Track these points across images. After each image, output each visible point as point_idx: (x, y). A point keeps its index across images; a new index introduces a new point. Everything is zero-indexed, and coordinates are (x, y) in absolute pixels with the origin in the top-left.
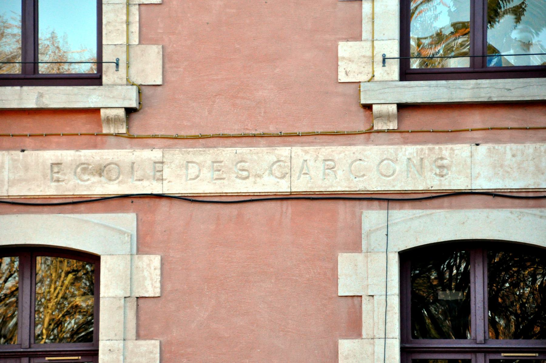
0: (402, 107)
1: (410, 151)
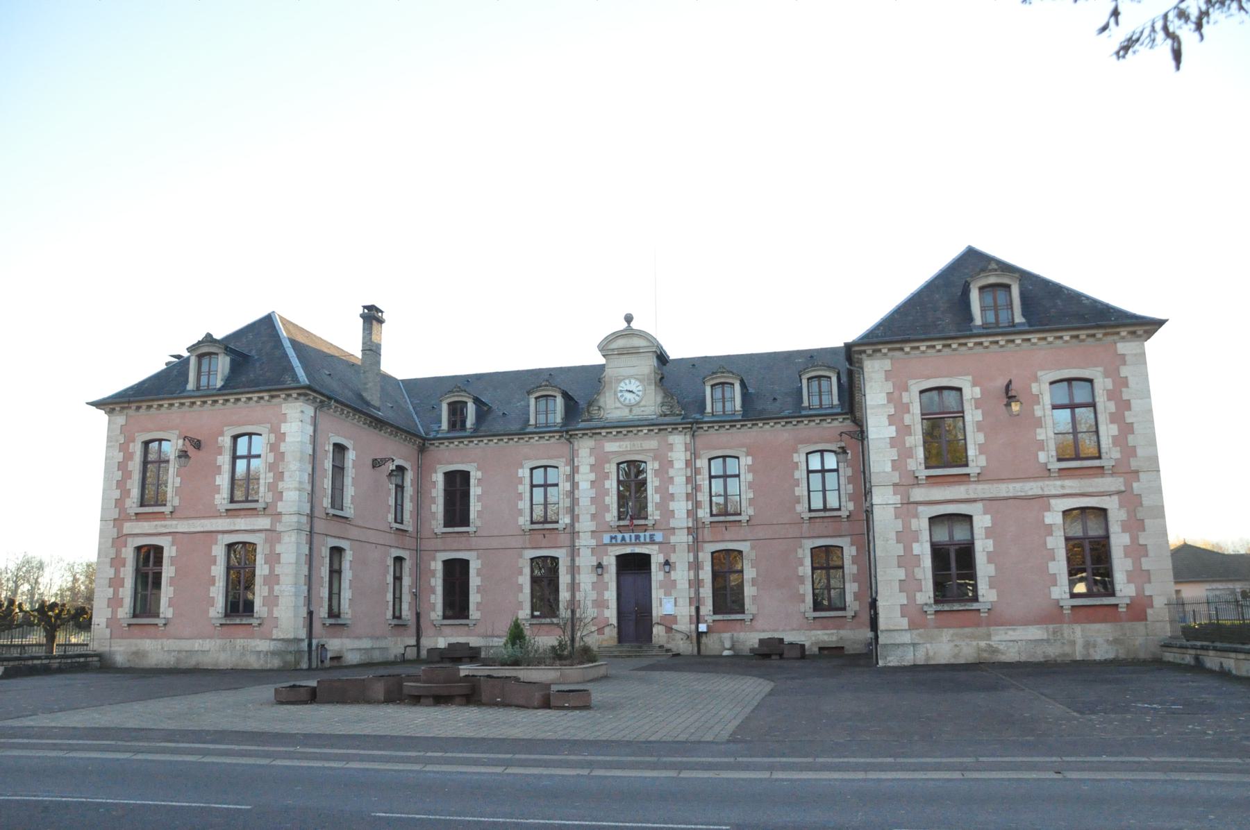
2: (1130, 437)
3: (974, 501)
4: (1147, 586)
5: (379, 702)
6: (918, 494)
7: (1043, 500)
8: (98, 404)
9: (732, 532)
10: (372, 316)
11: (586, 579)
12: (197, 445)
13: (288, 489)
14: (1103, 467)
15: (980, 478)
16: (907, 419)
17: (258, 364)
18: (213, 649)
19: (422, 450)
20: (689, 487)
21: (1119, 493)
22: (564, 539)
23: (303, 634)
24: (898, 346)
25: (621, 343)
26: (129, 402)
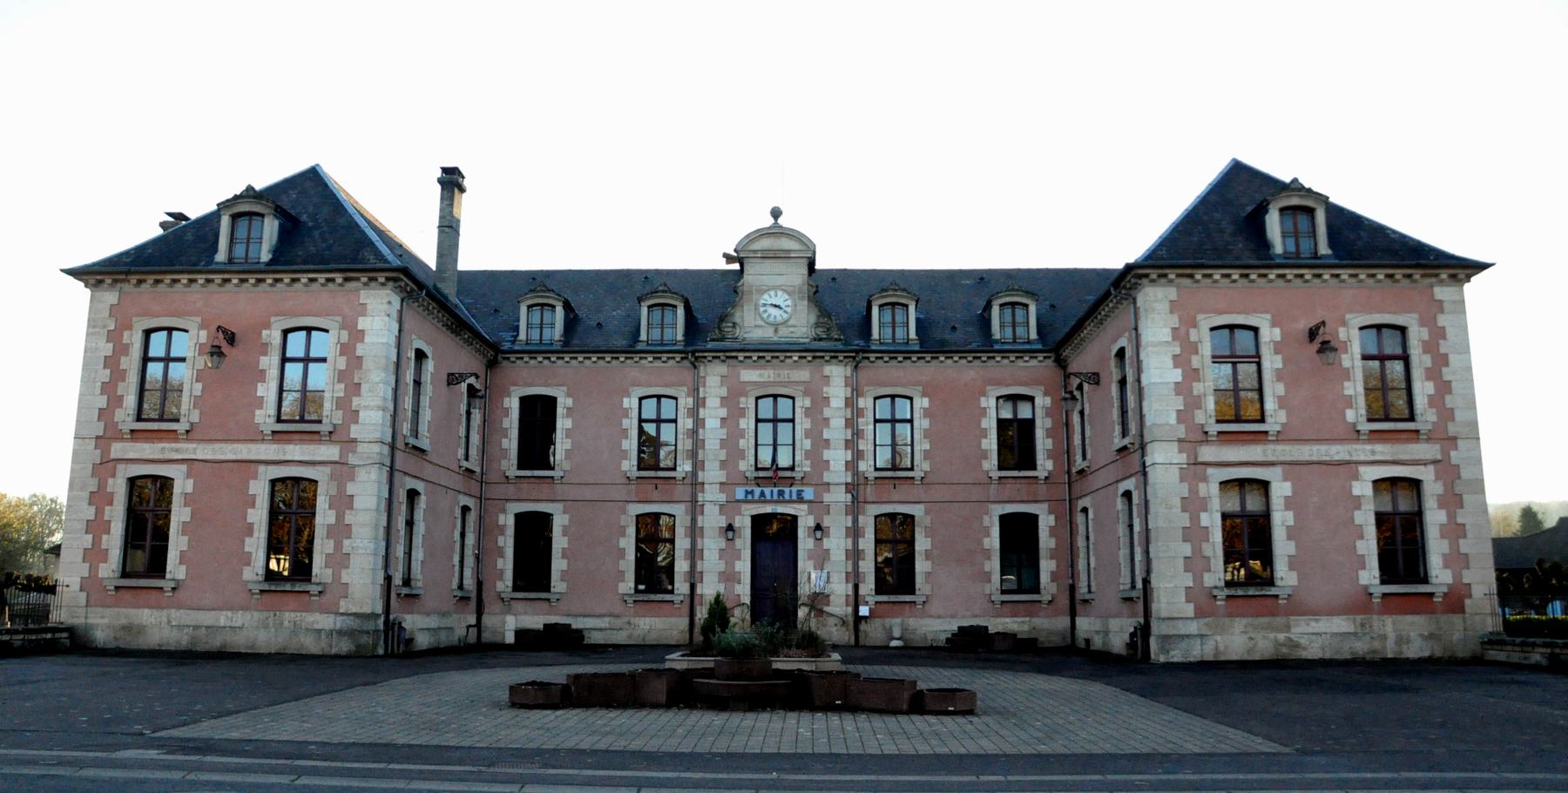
1: (275, 446)
2: (1448, 398)
3: (1272, 464)
4: (1465, 572)
5: (655, 706)
6: (1208, 453)
7: (1350, 467)
8: (75, 273)
9: (903, 491)
10: (451, 181)
11: (712, 545)
12: (231, 338)
13: (366, 407)
14: (1266, 433)
15: (1280, 438)
16: (1195, 362)
17: (316, 234)
18: (250, 627)
19: (492, 364)
20: (849, 432)
21: (1435, 462)
22: (682, 491)
23: (379, 609)
24: (1189, 271)
25: (765, 243)
26: (128, 273)
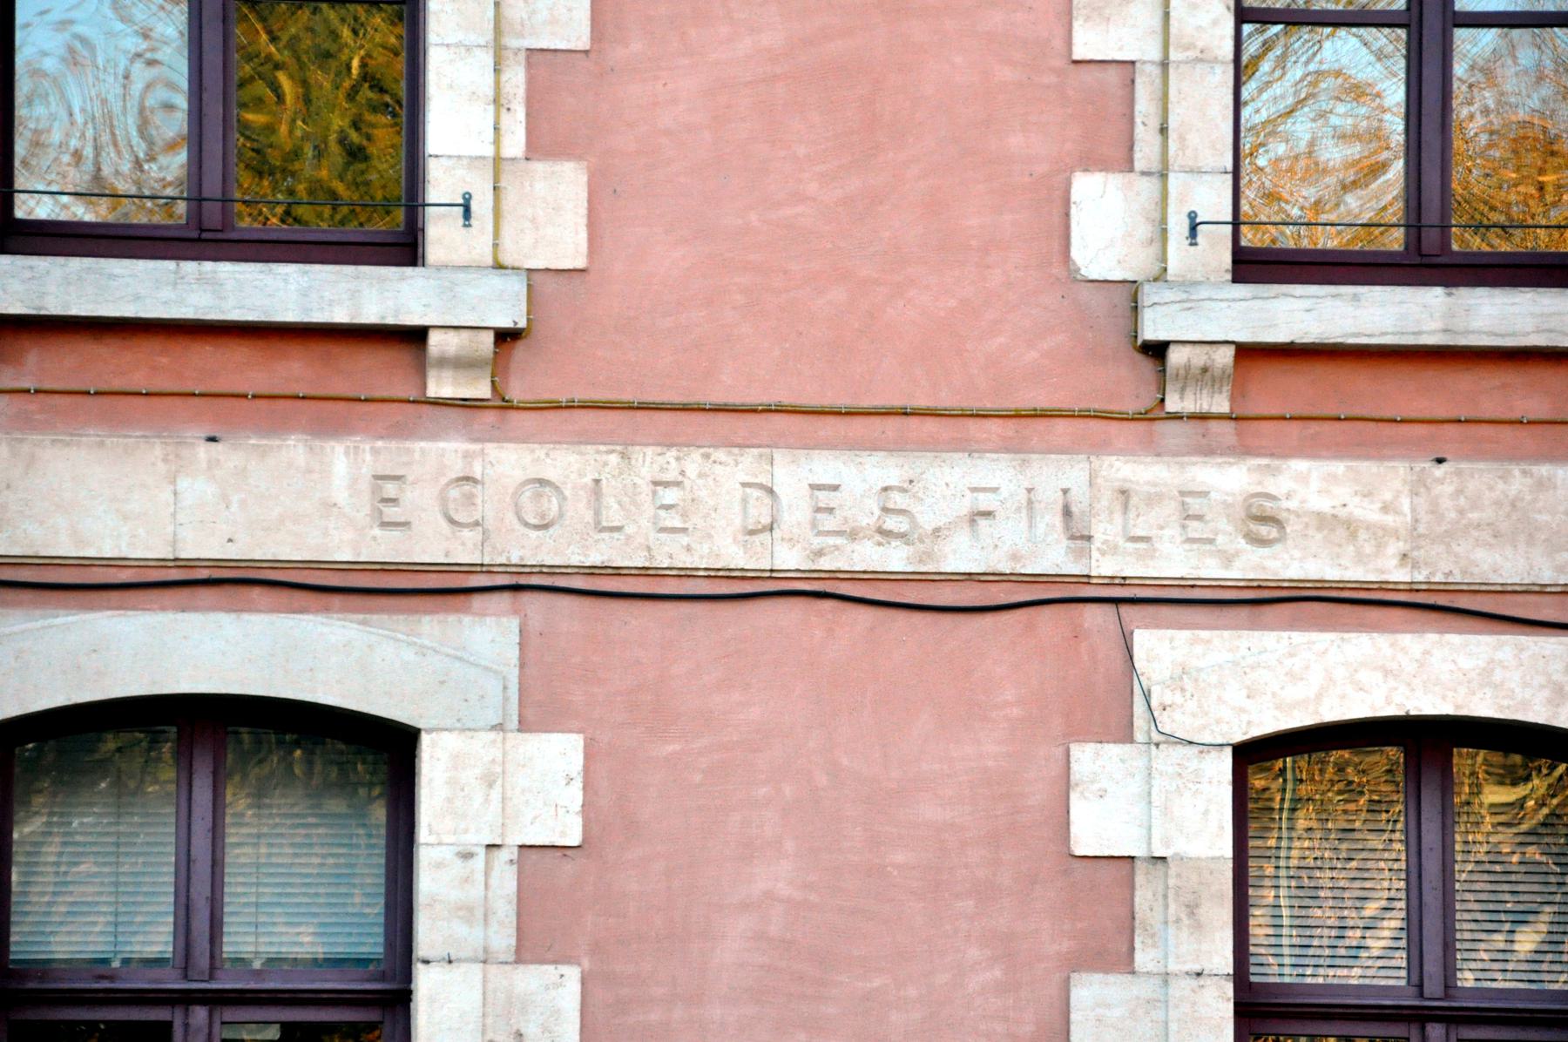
0: (1248, 353)
